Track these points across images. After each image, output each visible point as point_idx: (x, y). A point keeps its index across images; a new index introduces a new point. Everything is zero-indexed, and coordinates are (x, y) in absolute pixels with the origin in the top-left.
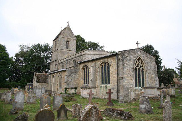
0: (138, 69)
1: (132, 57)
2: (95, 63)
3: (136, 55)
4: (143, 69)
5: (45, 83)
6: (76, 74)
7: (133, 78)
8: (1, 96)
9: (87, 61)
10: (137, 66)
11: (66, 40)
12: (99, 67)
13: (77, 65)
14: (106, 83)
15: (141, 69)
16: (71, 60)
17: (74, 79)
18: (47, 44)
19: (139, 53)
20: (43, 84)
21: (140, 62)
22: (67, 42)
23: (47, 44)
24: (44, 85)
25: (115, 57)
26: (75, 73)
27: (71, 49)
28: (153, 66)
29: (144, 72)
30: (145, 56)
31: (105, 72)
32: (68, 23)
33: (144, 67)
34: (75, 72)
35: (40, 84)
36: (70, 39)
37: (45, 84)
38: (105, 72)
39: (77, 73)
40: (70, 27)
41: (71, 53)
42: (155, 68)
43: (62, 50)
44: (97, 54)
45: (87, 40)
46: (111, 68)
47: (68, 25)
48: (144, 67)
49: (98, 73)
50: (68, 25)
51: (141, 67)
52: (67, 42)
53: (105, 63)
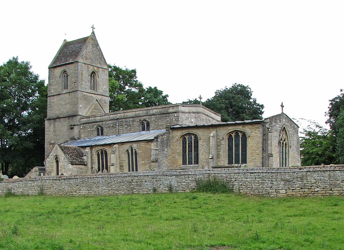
2: (217, 131)
5: (82, 165)
7: (180, 143)
8: (25, 248)
9: (212, 125)
11: (91, 69)
14: (237, 162)
16: (131, 119)
18: (134, 71)
23: (27, 63)
24: (81, 169)
25: (260, 126)
26: (167, 145)
27: (100, 91)
29: (287, 148)
31: (237, 146)
35: (75, 166)
36: (98, 67)
38: (237, 146)
41: (101, 100)
44: (194, 113)
46: (250, 143)
47: (93, 33)
50: (93, 33)
51: (284, 141)
53: (237, 132)
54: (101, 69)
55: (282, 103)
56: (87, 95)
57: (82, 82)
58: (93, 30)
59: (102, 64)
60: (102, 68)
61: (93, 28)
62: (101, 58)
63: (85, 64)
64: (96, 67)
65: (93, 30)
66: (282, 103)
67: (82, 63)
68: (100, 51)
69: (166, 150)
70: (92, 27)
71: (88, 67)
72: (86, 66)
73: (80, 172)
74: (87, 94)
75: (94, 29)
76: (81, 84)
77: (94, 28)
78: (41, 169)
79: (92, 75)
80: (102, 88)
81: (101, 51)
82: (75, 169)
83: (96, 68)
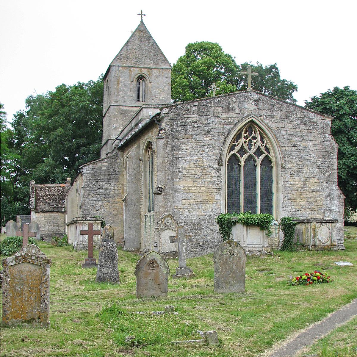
0: (242, 164)
1: (216, 121)
3: (233, 115)
4: (267, 161)
5: (57, 212)
6: (112, 181)
7: (219, 190)
10: (242, 151)
11: (136, 72)
12: (143, 158)
13: (116, 155)
15: (259, 161)
17: (106, 198)
19: (247, 106)
20: (51, 217)
21: (254, 138)
22: (141, 79)
24: (54, 218)
26: (109, 180)
28: (318, 148)
30: (277, 114)
32: (142, 14)
33: (275, 153)
34: (110, 175)
36: (151, 69)
37: (55, 214)
39: (116, 180)
40: (148, 28)
42: (327, 155)
43: (121, 107)
45: (96, 79)
47: (142, 22)
48: (275, 153)
49: (223, 182)
50: (142, 22)
51: (259, 152)
52: (141, 79)
54: (155, 70)
55: (142, 10)
56: (127, 111)
57: (118, 93)
58: (142, 17)
59: (160, 63)
60: (158, 68)
61: (142, 15)
62: (158, 54)
63: (123, 67)
64: (146, 68)
65: (142, 17)
66: (142, 10)
67: (118, 66)
68: (154, 44)
69: (105, 187)
70: (144, 15)
71: (130, 70)
72: (126, 71)
73: (51, 223)
74: (128, 108)
75: (141, 13)
76: (117, 96)
77: (144, 15)
78: (25, 218)
79: (141, 81)
80: (157, 98)
81: (156, 44)
82: (43, 219)
83: (145, 72)
